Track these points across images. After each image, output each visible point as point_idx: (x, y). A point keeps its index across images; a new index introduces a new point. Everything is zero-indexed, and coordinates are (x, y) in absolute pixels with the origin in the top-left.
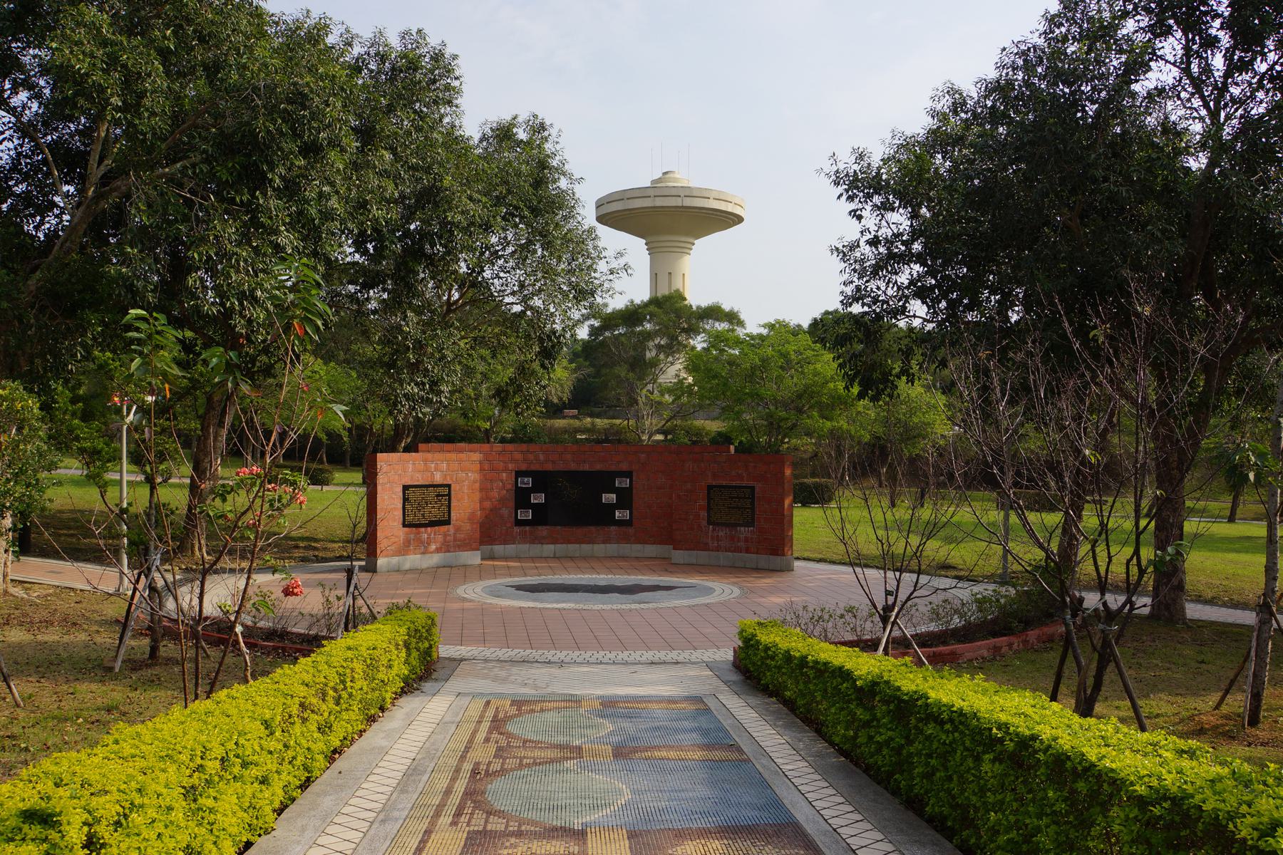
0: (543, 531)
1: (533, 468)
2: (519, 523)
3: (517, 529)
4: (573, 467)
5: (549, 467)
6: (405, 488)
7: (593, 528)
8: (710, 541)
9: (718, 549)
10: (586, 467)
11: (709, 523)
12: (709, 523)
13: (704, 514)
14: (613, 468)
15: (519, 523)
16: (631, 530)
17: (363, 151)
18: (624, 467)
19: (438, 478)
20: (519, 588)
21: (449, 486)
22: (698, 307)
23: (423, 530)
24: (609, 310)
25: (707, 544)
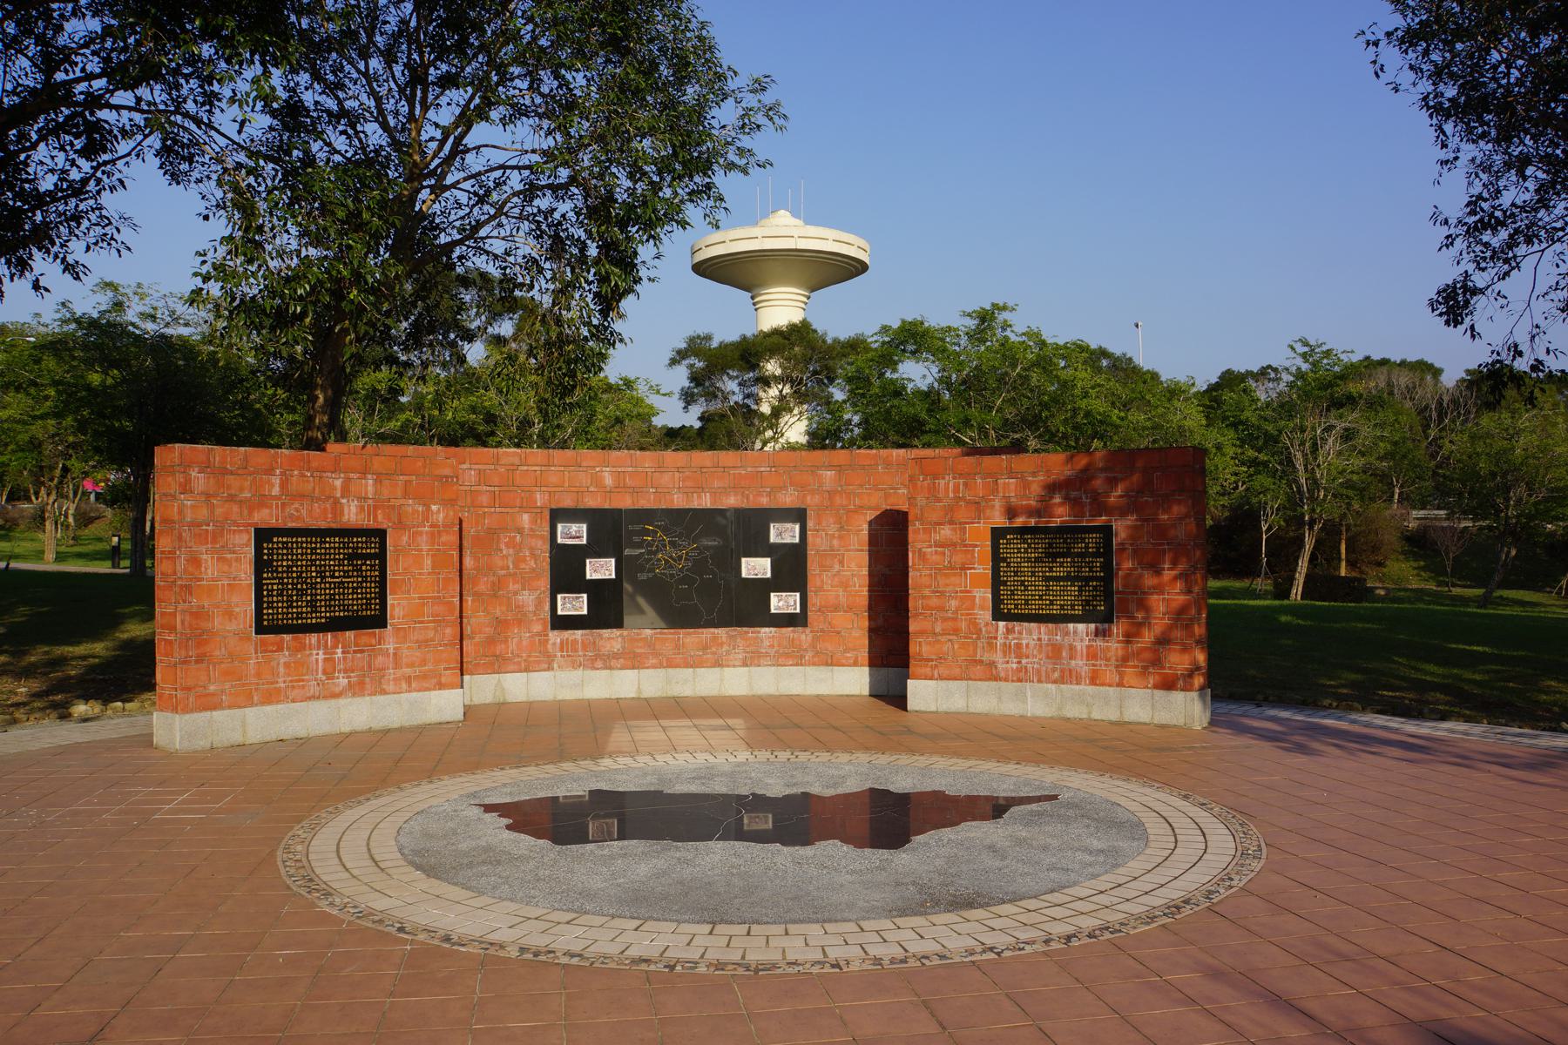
0: (611, 639)
1: (591, 502)
2: (562, 623)
3: (556, 637)
4: (678, 501)
5: (625, 502)
6: (263, 535)
7: (721, 632)
8: (998, 658)
9: (1021, 676)
10: (706, 502)
11: (998, 615)
12: (998, 615)
13: (984, 595)
14: (764, 502)
15: (562, 623)
16: (802, 636)
17: (350, 35)
18: (788, 499)
19: (352, 515)
20: (527, 817)
21: (381, 534)
22: (836, 341)
23: (313, 638)
24: (715, 344)
25: (992, 664)
